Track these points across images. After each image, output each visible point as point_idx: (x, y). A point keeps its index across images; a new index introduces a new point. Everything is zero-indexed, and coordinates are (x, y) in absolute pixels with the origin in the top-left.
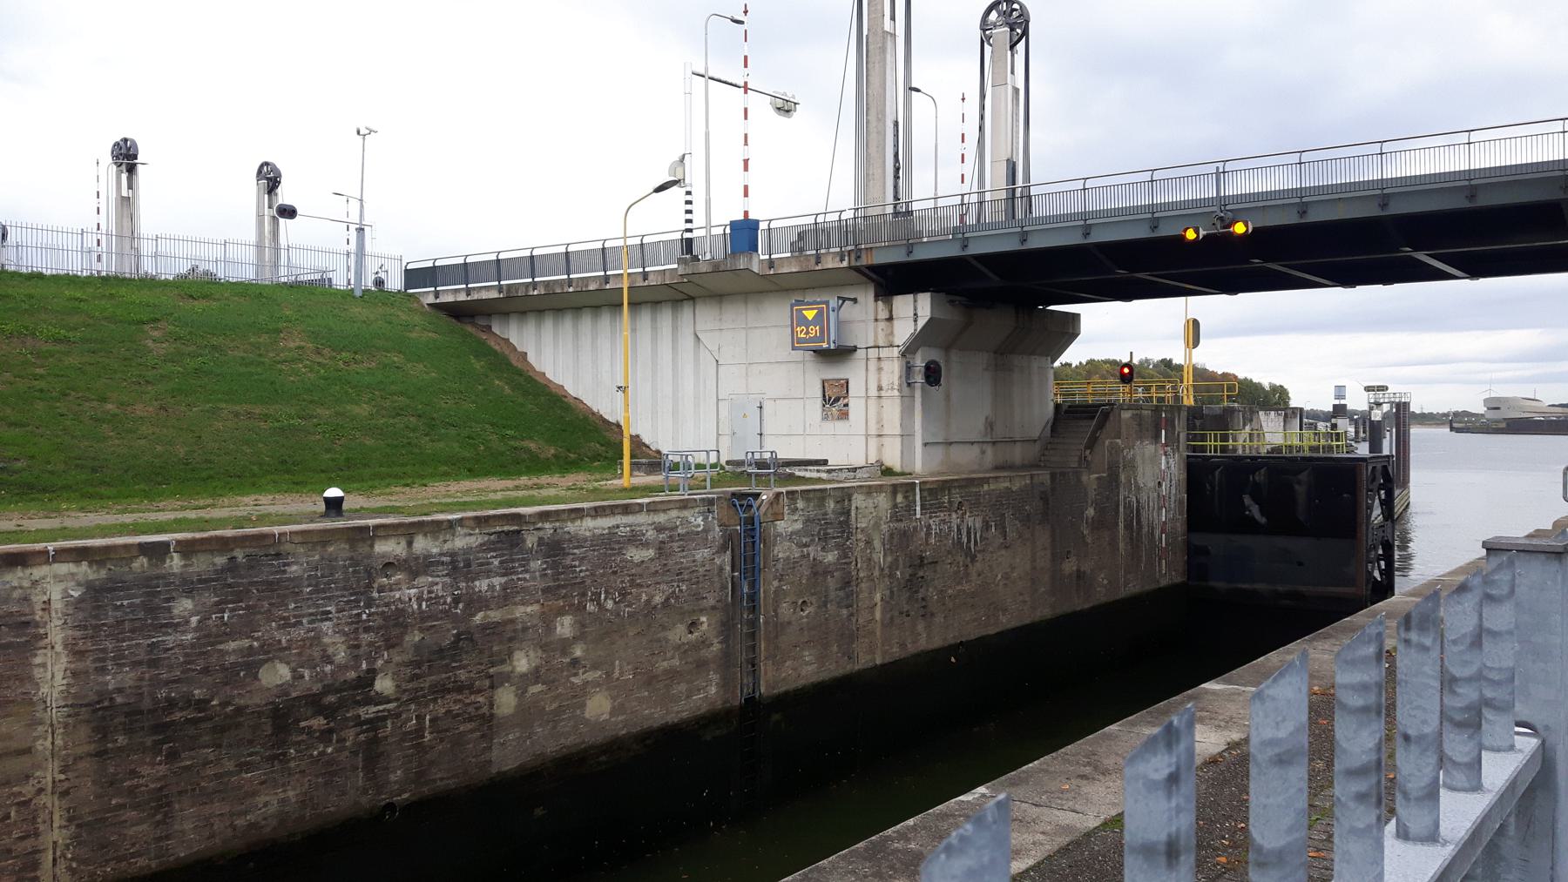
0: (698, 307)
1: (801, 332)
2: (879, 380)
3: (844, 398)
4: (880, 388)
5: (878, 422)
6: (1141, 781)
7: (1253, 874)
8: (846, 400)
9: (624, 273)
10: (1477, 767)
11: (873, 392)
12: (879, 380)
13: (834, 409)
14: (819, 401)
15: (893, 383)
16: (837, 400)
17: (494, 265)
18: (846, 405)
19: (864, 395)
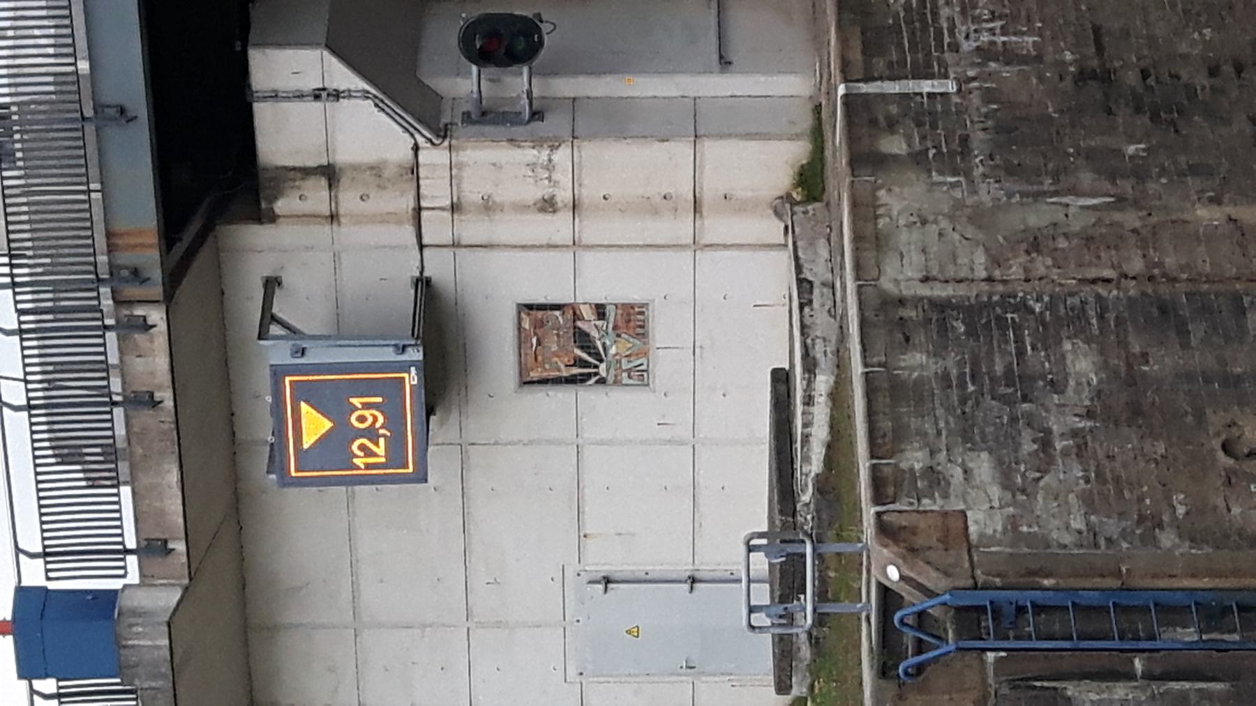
2: (522, 208)
3: (577, 316)
4: (548, 205)
5: (655, 212)
8: (587, 312)
11: (559, 227)
12: (522, 208)
13: (613, 351)
14: (589, 395)
15: (532, 166)
16: (583, 339)
18: (600, 310)
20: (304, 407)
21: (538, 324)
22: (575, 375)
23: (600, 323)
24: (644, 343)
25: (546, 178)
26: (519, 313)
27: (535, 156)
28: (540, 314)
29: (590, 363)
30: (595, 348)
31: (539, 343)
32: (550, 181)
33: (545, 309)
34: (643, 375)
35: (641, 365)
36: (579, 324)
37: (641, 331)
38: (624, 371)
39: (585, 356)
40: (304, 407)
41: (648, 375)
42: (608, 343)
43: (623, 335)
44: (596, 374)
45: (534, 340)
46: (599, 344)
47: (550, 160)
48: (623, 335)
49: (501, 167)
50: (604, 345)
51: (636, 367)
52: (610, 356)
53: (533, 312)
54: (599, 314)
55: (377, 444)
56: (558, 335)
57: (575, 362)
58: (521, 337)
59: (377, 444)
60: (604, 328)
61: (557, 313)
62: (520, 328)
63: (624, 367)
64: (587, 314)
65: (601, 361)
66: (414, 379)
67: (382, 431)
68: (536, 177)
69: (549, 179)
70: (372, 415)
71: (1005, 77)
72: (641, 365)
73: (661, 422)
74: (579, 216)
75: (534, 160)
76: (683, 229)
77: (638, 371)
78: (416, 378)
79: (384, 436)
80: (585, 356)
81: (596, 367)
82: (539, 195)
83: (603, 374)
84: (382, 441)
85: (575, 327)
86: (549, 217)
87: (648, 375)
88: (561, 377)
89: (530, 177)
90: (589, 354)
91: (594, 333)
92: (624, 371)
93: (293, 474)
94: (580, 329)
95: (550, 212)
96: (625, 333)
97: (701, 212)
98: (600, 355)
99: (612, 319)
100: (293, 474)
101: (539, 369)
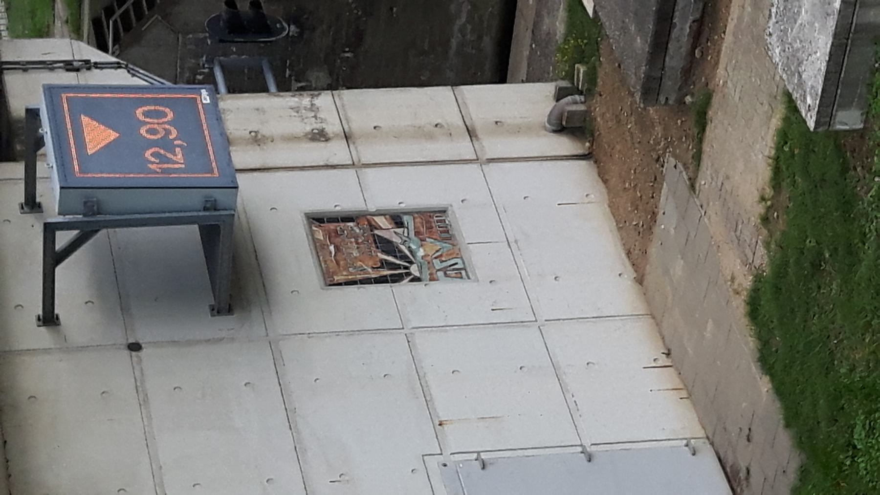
0: (17, 346)
1: (163, 159)
2: (293, 139)
3: (373, 227)
4: (320, 136)
5: (430, 137)
6: (873, 171)
7: (817, 2)
8: (381, 221)
9: (82, 11)
10: (580, 8)
11: (337, 152)
12: (293, 139)
13: (421, 253)
14: (405, 288)
15: (297, 109)
16: (387, 246)
17: (62, 190)
18: (397, 220)
19: (352, 172)
20: (85, 119)
21: (332, 236)
22: (386, 276)
23: (400, 230)
24: (453, 245)
25: (313, 117)
26: (311, 227)
27: (297, 102)
28: (332, 226)
29: (399, 265)
30: (400, 251)
31: (337, 248)
32: (316, 119)
33: (338, 222)
34: (461, 273)
35: (456, 264)
36: (376, 232)
37: (446, 234)
38: (439, 270)
39: (391, 259)
40: (85, 119)
41: (466, 272)
42: (413, 247)
43: (427, 239)
44: (409, 274)
45: (332, 248)
46: (403, 248)
47: (312, 105)
48: (427, 239)
49: (264, 112)
50: (409, 248)
51: (450, 266)
52: (419, 259)
53: (326, 225)
54: (396, 223)
55: (175, 155)
56: (357, 243)
57: (382, 264)
58: (318, 248)
59: (175, 155)
60: (406, 234)
61: (351, 224)
62: (315, 240)
63: (438, 268)
64: (384, 224)
65: (411, 263)
66: (205, 99)
67: (176, 142)
68: (302, 116)
69: (315, 117)
70: (165, 129)
71: (774, 214)
72: (456, 264)
73: (494, 308)
74: (354, 143)
75: (297, 105)
76: (465, 148)
77: (454, 270)
78: (208, 98)
79: (178, 146)
80: (391, 259)
81: (406, 268)
82: (308, 129)
83: (417, 274)
84: (178, 150)
85: (374, 235)
86: (322, 144)
87: (466, 272)
88: (370, 279)
89: (295, 116)
90: (396, 257)
91: (396, 240)
92: (439, 270)
93: (78, 175)
94: (377, 235)
95: (323, 141)
96: (429, 238)
97: (476, 136)
98: (408, 257)
99: (411, 227)
100: (78, 175)
101: (345, 273)
